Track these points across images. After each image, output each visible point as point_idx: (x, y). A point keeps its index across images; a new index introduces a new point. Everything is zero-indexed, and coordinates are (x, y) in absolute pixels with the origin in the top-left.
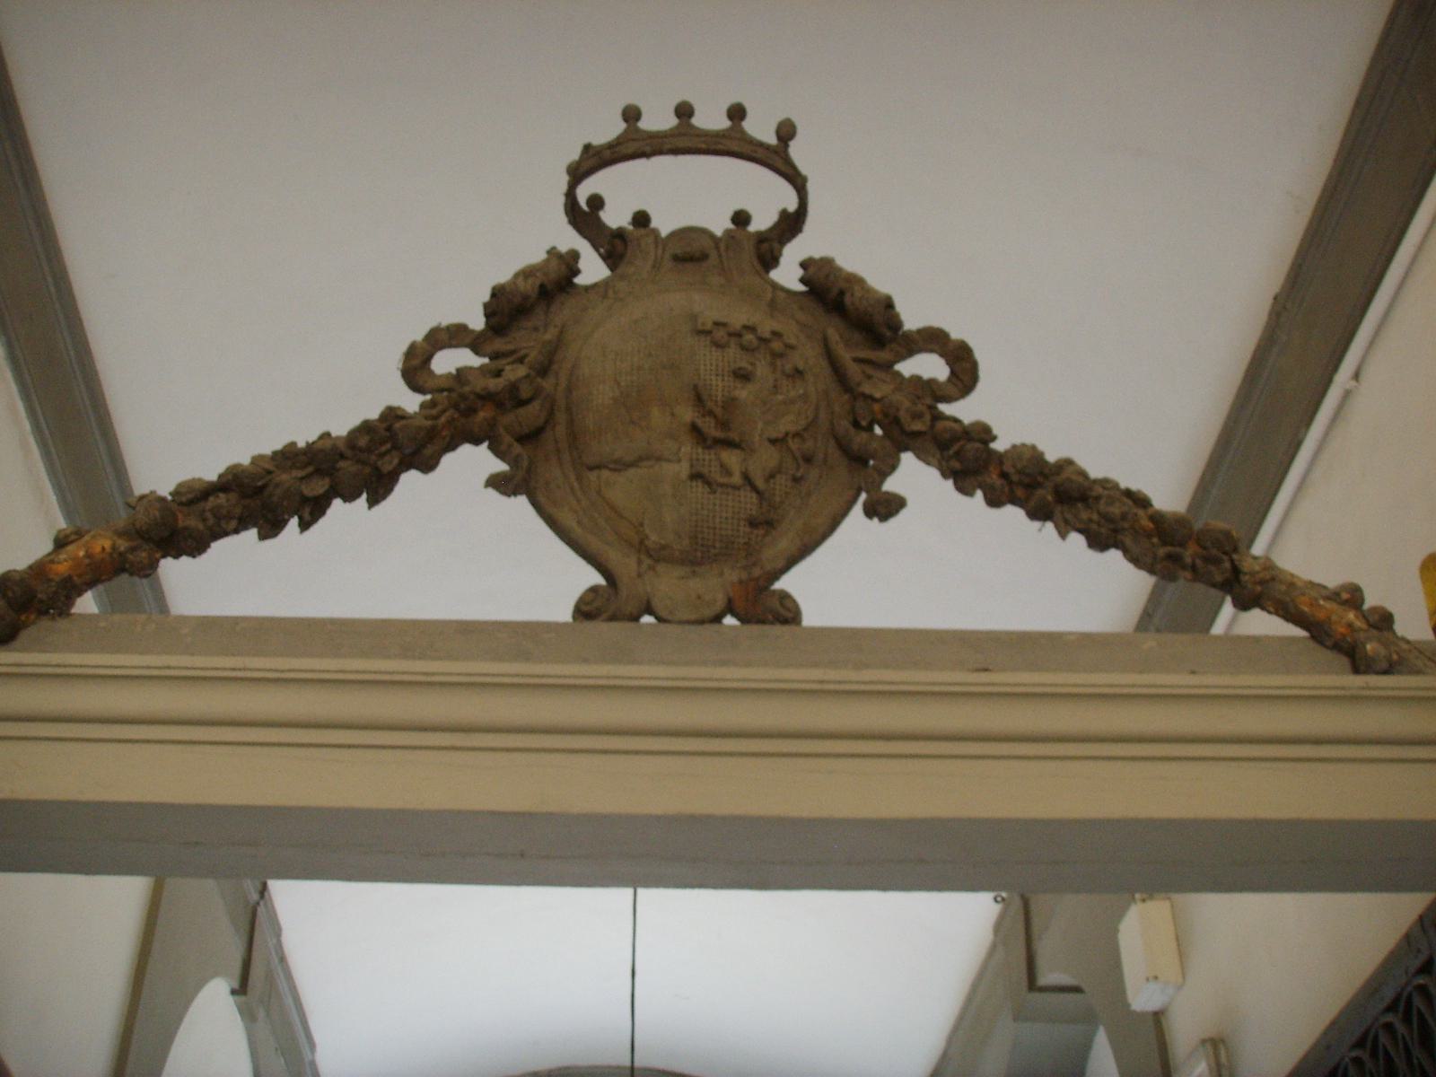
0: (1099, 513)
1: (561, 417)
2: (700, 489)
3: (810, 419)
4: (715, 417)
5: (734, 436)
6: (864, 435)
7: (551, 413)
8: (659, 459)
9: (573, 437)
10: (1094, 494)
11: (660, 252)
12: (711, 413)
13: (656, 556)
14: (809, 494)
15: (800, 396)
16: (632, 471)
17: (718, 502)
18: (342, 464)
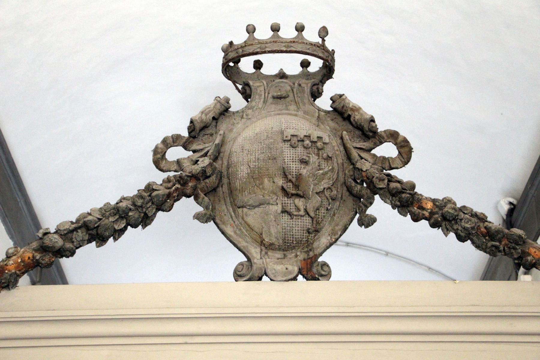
0: (462, 227)
1: (225, 181)
2: (286, 218)
3: (334, 180)
4: (292, 182)
5: (300, 193)
6: (359, 187)
7: (220, 180)
8: (269, 204)
9: (231, 191)
10: (460, 218)
11: (266, 94)
12: (290, 181)
13: (268, 247)
14: (334, 215)
15: (330, 170)
16: (257, 209)
17: (294, 223)
18: (130, 214)
